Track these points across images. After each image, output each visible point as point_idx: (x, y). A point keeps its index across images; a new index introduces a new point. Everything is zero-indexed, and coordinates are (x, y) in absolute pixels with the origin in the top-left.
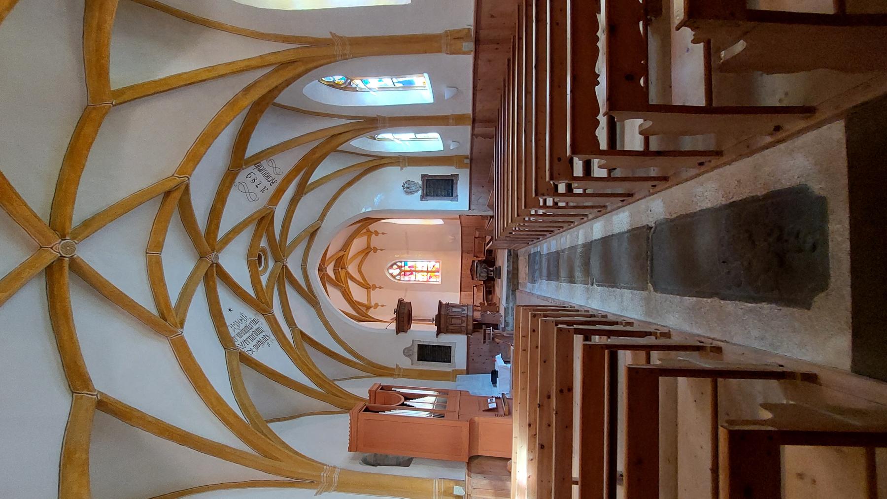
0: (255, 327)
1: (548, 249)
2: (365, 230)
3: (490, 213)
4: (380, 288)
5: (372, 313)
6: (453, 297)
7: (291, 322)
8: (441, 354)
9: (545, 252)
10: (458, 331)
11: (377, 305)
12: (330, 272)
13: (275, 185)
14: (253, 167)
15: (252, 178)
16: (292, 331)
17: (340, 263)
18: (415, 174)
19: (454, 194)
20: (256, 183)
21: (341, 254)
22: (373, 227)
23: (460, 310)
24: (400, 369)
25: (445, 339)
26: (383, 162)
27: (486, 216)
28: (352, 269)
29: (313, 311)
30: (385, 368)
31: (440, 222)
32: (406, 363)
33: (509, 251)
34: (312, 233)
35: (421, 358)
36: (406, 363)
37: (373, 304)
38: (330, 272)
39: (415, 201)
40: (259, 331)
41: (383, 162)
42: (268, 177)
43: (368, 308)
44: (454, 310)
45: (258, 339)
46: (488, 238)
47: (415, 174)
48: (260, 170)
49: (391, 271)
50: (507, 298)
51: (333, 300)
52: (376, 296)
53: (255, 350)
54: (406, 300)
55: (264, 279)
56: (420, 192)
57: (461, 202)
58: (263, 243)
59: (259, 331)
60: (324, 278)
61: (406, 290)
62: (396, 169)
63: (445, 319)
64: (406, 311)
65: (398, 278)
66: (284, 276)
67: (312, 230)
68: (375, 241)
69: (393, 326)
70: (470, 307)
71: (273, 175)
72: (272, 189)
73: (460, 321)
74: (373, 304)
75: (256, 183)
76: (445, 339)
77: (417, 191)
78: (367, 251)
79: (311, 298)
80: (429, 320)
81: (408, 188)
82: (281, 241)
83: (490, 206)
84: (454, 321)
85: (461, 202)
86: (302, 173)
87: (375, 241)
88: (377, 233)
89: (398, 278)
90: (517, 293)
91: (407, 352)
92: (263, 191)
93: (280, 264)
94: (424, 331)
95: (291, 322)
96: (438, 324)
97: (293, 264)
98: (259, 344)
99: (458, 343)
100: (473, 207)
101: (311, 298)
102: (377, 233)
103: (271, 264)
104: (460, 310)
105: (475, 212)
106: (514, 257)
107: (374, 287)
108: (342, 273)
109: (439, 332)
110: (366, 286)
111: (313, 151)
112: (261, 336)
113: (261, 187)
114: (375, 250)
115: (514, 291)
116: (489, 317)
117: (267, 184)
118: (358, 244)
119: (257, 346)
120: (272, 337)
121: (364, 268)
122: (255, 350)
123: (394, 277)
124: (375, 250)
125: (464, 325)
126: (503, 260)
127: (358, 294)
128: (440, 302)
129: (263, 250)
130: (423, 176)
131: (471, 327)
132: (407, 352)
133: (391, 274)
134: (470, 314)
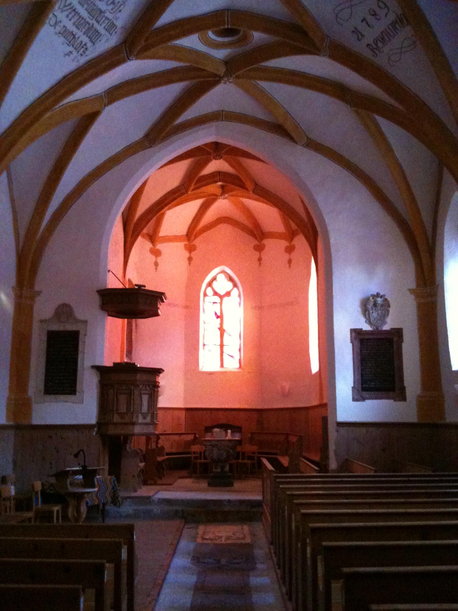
0: (101, 29)
1: (260, 589)
2: (294, 226)
3: (333, 465)
4: (190, 259)
5: (141, 245)
6: (172, 394)
7: (115, 94)
8: (62, 378)
9: (255, 580)
10: (105, 406)
11: (156, 253)
12: (215, 165)
13: (367, 54)
14: (400, 12)
15: (378, 10)
16: (97, 98)
17: (232, 183)
18: (402, 316)
19: (365, 394)
20: (369, 18)
21: (249, 184)
22: (301, 242)
23: (145, 408)
24: (32, 298)
25: (89, 385)
26: (424, 255)
27: (325, 457)
28: (223, 205)
29: (138, 134)
30: (34, 271)
31: (315, 367)
32: (44, 309)
33: (258, 504)
34: (281, 128)
35: (53, 338)
36: (44, 309)
37: (159, 246)
38: (215, 165)
39: (348, 319)
40: (94, 36)
41: (424, 255)
42: (383, 38)
43: (152, 238)
44: (145, 398)
45: (79, 33)
46: (285, 461)
47: (402, 316)
48: (393, 24)
49: (221, 278)
50: (168, 502)
51: (160, 174)
52: (174, 255)
53: (58, 29)
54: (162, 309)
55: (191, 41)
56: (366, 327)
57: (348, 406)
58: (258, 37)
59: (94, 36)
60: (201, 154)
61: (187, 307)
62: (411, 281)
63: (130, 382)
64: (142, 307)
65: (209, 291)
66: (199, 78)
67: (288, 126)
68: (275, 248)
69: (113, 283)
70: (150, 429)
71: (386, 49)
72: (360, 48)
73: (123, 409)
74: (159, 246)
75: (369, 18)
76: (89, 385)
77: (369, 322)
78: (257, 233)
79: (160, 132)
80: (129, 352)
81: (371, 305)
82: (267, 70)
83: (345, 465)
84: (123, 399)
85: (348, 406)
86: (392, 101)
87: (275, 248)
88: (290, 249)
89: (209, 291)
90: (177, 523)
91: (64, 311)
92: (356, 31)
93: (222, 70)
94: (106, 342)
95: (115, 94)
96: (119, 368)
97: (224, 95)
98: (69, 37)
99: (82, 409)
100: (343, 430)
101: (160, 132)
102: (290, 249)
103: (221, 54)
104: (145, 408)
105: (332, 434)
106: (245, 513)
107: (191, 249)
108: (214, 188)
109: (101, 370)
110: (192, 234)
111: (438, 123)
112: (85, 39)
113: (362, 27)
114: (259, 248)
115: (175, 515)
116: (133, 466)
117: (369, 39)
118: (268, 215)
119: (66, 34)
120: (83, 60)
121: (225, 229)
122: (58, 29)
123: (210, 284)
124: (259, 248)
125: (116, 419)
126: (248, 491)
127: (177, 219)
128: (158, 371)
129: (245, 39)
130: (398, 333)
131: (112, 431)
132: (64, 311)
133: (214, 279)
134: (137, 429)
